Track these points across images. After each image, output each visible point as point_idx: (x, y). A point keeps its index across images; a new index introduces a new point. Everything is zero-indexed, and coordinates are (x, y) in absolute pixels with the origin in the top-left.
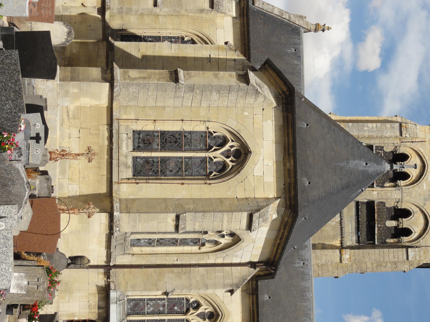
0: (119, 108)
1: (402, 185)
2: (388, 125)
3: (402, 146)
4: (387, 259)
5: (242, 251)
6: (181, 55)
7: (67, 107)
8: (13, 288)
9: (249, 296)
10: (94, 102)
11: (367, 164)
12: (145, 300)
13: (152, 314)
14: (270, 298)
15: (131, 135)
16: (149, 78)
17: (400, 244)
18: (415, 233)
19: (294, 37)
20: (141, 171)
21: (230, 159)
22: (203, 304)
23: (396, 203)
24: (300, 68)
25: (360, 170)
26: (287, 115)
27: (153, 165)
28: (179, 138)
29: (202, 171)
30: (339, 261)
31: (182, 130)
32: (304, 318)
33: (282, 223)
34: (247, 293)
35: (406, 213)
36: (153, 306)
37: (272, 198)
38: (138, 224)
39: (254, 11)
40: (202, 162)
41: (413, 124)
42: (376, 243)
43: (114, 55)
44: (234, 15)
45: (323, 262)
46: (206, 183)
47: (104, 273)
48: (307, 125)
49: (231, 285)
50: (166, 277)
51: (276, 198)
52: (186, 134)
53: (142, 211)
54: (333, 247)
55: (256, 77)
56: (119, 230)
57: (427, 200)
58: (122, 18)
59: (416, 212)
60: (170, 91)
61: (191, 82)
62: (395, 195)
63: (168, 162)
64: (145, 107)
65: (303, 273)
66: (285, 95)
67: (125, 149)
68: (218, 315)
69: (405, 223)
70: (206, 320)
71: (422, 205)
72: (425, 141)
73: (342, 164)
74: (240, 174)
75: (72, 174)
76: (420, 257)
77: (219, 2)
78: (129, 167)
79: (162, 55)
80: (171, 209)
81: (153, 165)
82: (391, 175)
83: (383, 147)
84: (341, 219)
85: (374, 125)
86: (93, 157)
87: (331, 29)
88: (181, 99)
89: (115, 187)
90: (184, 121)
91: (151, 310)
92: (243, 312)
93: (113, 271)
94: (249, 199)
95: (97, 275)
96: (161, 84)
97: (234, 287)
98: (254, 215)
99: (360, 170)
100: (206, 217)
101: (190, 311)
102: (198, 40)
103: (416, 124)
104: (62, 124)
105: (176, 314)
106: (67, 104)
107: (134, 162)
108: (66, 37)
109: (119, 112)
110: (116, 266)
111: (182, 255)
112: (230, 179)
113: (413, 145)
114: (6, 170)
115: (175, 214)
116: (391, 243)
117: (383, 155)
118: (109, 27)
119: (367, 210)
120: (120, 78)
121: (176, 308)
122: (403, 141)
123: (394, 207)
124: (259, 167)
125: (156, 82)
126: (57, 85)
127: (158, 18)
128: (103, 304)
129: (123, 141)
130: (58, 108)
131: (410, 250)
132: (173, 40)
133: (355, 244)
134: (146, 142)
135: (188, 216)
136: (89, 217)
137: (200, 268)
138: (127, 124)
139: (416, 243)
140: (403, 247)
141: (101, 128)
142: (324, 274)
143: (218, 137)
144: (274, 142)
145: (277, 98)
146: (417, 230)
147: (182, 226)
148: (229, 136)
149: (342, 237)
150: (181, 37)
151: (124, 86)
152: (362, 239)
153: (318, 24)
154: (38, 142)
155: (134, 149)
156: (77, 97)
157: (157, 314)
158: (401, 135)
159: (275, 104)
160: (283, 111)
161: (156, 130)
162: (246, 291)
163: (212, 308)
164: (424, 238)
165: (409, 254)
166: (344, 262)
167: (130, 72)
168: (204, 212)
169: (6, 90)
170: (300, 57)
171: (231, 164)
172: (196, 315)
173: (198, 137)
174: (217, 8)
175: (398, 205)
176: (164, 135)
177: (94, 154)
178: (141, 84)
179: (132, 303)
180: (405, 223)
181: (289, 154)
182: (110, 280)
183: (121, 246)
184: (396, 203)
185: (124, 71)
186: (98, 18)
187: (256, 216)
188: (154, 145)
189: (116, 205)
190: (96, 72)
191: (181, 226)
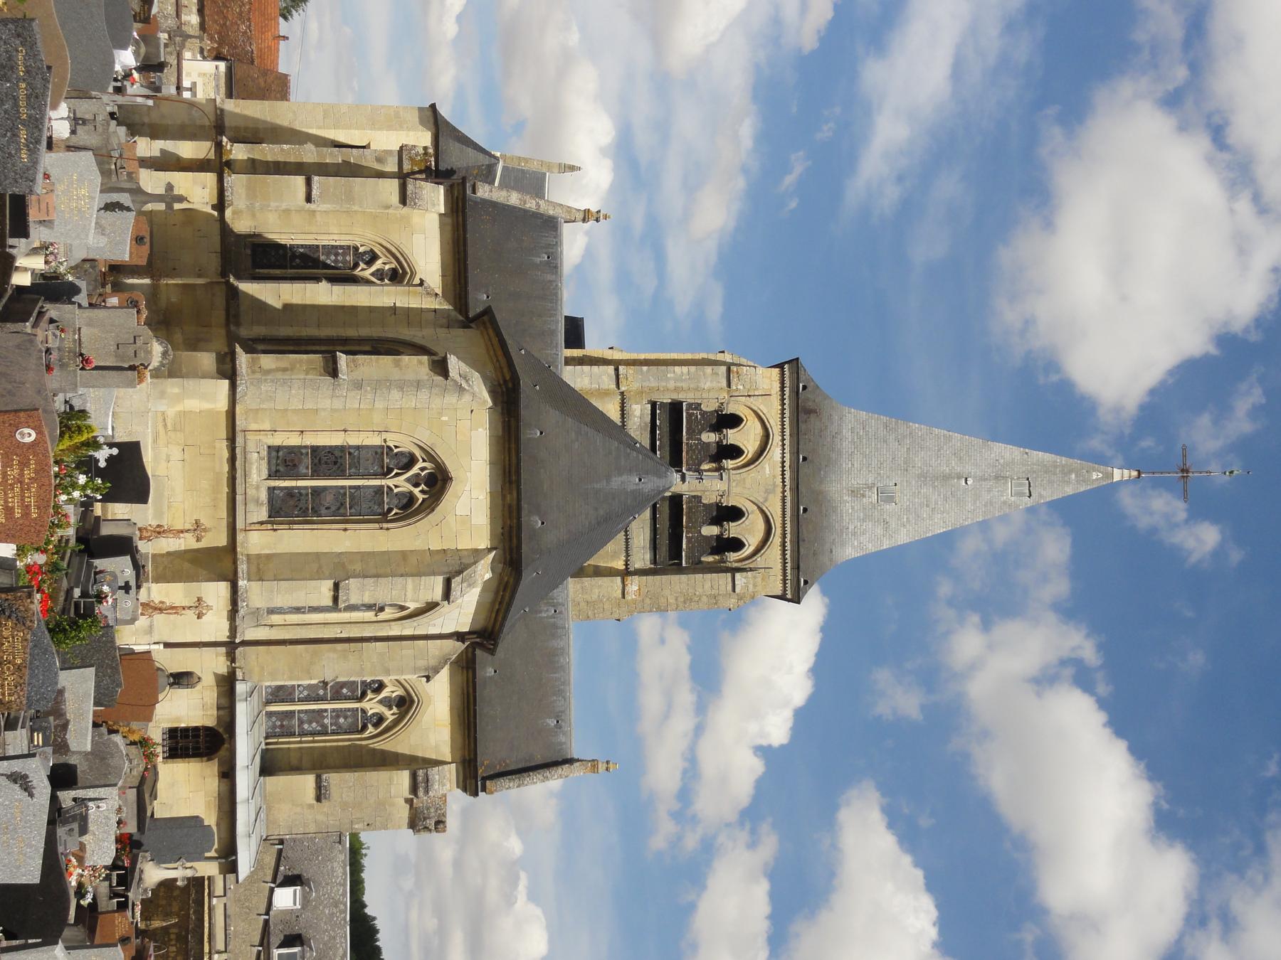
0: (246, 413)
1: (730, 467)
2: (708, 369)
3: (732, 402)
4: (699, 591)
5: (442, 619)
6: (347, 303)
7: (163, 413)
9: (463, 671)
10: (206, 406)
11: (640, 480)
13: (306, 701)
14: (495, 672)
15: (264, 453)
16: (292, 369)
17: (724, 565)
18: (749, 545)
19: (547, 235)
20: (281, 509)
21: (420, 488)
22: (387, 684)
23: (719, 498)
24: (557, 285)
25: (629, 490)
26: (509, 421)
27: (299, 500)
28: (341, 457)
29: (376, 507)
30: (621, 596)
31: (345, 444)
32: (555, 698)
33: (500, 583)
34: (459, 666)
35: (735, 514)
37: (484, 549)
38: (276, 595)
39: (476, 203)
41: (750, 366)
42: (684, 564)
43: (238, 305)
44: (442, 210)
45: (595, 597)
46: (381, 529)
47: (227, 653)
48: (541, 433)
49: (426, 669)
50: (323, 657)
51: (490, 550)
52: (352, 451)
53: (281, 577)
54: (611, 573)
55: (460, 362)
56: (246, 605)
57: (769, 493)
58: (254, 216)
59: (753, 512)
61: (357, 375)
62: (717, 485)
63: (324, 494)
64: (286, 410)
65: (555, 626)
66: (507, 388)
68: (412, 702)
69: (733, 529)
70: (392, 709)
73: (597, 486)
74: (435, 512)
75: (174, 518)
76: (755, 586)
77: (416, 193)
78: (262, 504)
79: (316, 303)
80: (327, 573)
81: (299, 500)
82: (713, 450)
83: (701, 404)
85: (685, 369)
86: (203, 534)
88: (343, 399)
90: (349, 432)
91: (305, 694)
93: (239, 651)
94: (449, 552)
95: (214, 657)
98: (453, 580)
99: (629, 490)
100: (380, 583)
101: (367, 695)
102: (382, 253)
103: (756, 365)
104: (155, 441)
105: (345, 700)
106: (162, 408)
107: (269, 494)
108: (160, 359)
109: (245, 419)
110: (245, 643)
111: (349, 625)
112: (419, 520)
113: (750, 401)
114: (104, 744)
115: (333, 581)
116: (708, 563)
117: (699, 417)
118: (232, 231)
119: (669, 509)
120: (247, 371)
121: (345, 691)
123: (717, 504)
124: (464, 499)
125: (302, 376)
127: (314, 215)
128: (224, 702)
129: (251, 464)
130: (150, 414)
131: (738, 576)
132: (340, 251)
133: (649, 565)
135: (353, 582)
136: (198, 618)
137: (378, 644)
138: (258, 438)
139: (749, 563)
140: (727, 570)
141: (218, 444)
142: (597, 616)
143: (402, 453)
144: (488, 462)
145: (493, 393)
146: (752, 542)
147: (344, 598)
148: (418, 453)
149: (628, 555)
150: (353, 247)
151: (252, 383)
152: (660, 558)
154: (127, 592)
155: (270, 476)
157: (314, 701)
158: (729, 385)
159: (490, 403)
160: (503, 414)
161: (303, 444)
163: (403, 690)
164: (762, 555)
165: (736, 583)
166: (628, 597)
167: (261, 360)
168: (377, 576)
169: (103, 667)
170: (556, 267)
171: (421, 497)
172: (377, 702)
173: (370, 454)
174: (413, 204)
177: (205, 530)
178: (278, 380)
180: (733, 529)
181: (510, 482)
182: (235, 664)
183: (251, 616)
184: (719, 498)
185: (252, 358)
186: (213, 215)
187: (456, 582)
188: (301, 468)
189: (242, 567)
190: (207, 360)
191: (342, 597)
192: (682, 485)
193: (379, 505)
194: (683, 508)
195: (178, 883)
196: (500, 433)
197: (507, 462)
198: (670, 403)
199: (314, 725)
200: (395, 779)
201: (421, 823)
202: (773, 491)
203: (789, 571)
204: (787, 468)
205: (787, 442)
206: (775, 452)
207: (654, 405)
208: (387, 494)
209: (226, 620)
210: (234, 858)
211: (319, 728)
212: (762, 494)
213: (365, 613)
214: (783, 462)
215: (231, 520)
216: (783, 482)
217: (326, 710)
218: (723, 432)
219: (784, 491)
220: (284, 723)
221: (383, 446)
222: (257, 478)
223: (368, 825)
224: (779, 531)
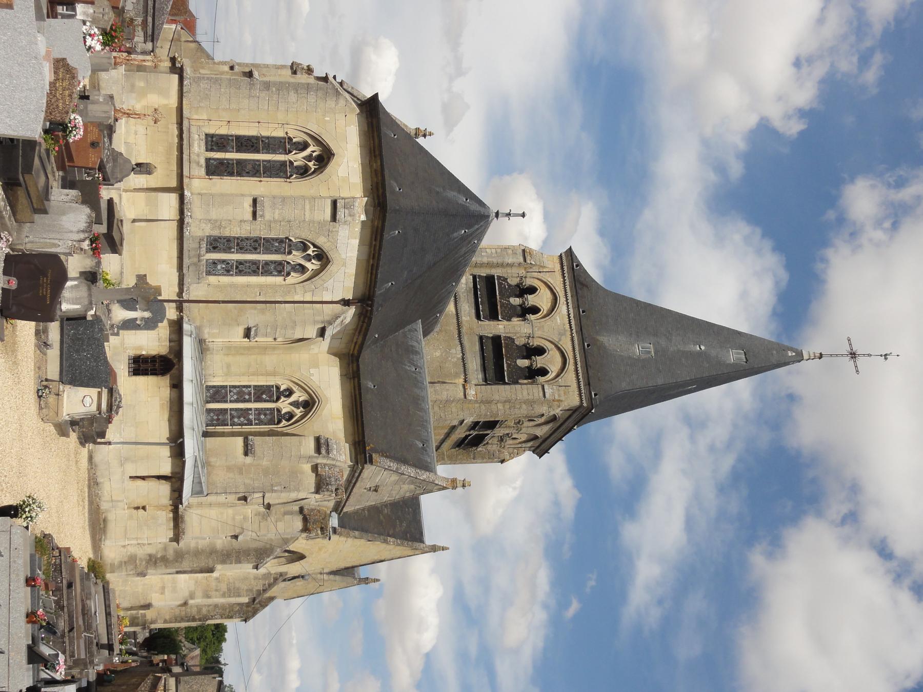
8: (80, 15)
10: (163, 101)
12: (227, 388)
15: (203, 137)
18: (552, 372)
23: (526, 340)
28: (256, 143)
31: (259, 135)
34: (347, 378)
35: (540, 351)
36: (238, 393)
40: (281, 165)
59: (552, 349)
60: (244, 89)
67: (197, 148)
72: (554, 272)
74: (323, 173)
84: (463, 354)
86: (159, 63)
87: (433, 134)
89: (186, 180)
92: (343, 398)
96: (234, 79)
97: (326, 324)
100: (286, 203)
117: (507, 287)
121: (264, 396)
122: (529, 271)
123: (525, 345)
126: (122, 74)
128: (174, 337)
134: (219, 145)
136: (155, 123)
141: (170, 126)
142: (447, 416)
143: (299, 143)
146: (554, 369)
148: (309, 141)
149: (466, 375)
153: (419, 128)
156: (143, 94)
158: (525, 260)
160: (367, 118)
162: (346, 375)
163: (307, 395)
165: (546, 391)
175: (529, 342)
176: (240, 139)
181: (375, 156)
184: (526, 340)
188: (229, 148)
191: (259, 213)
192: (500, 328)
193: (284, 173)
194: (502, 343)
195: (137, 322)
197: (372, 145)
198: (486, 277)
199: (242, 419)
200: (304, 442)
201: (325, 487)
202: (564, 334)
203: (582, 387)
204: (572, 318)
205: (570, 301)
206: (562, 308)
207: (474, 277)
208: (289, 166)
209: (176, 270)
210: (181, 440)
211: (246, 422)
212: (557, 336)
214: (569, 315)
215: (179, 171)
216: (571, 327)
217: (251, 409)
218: (524, 297)
219: (572, 334)
220: (220, 417)
221: (286, 138)
222: (198, 150)
224: (572, 361)
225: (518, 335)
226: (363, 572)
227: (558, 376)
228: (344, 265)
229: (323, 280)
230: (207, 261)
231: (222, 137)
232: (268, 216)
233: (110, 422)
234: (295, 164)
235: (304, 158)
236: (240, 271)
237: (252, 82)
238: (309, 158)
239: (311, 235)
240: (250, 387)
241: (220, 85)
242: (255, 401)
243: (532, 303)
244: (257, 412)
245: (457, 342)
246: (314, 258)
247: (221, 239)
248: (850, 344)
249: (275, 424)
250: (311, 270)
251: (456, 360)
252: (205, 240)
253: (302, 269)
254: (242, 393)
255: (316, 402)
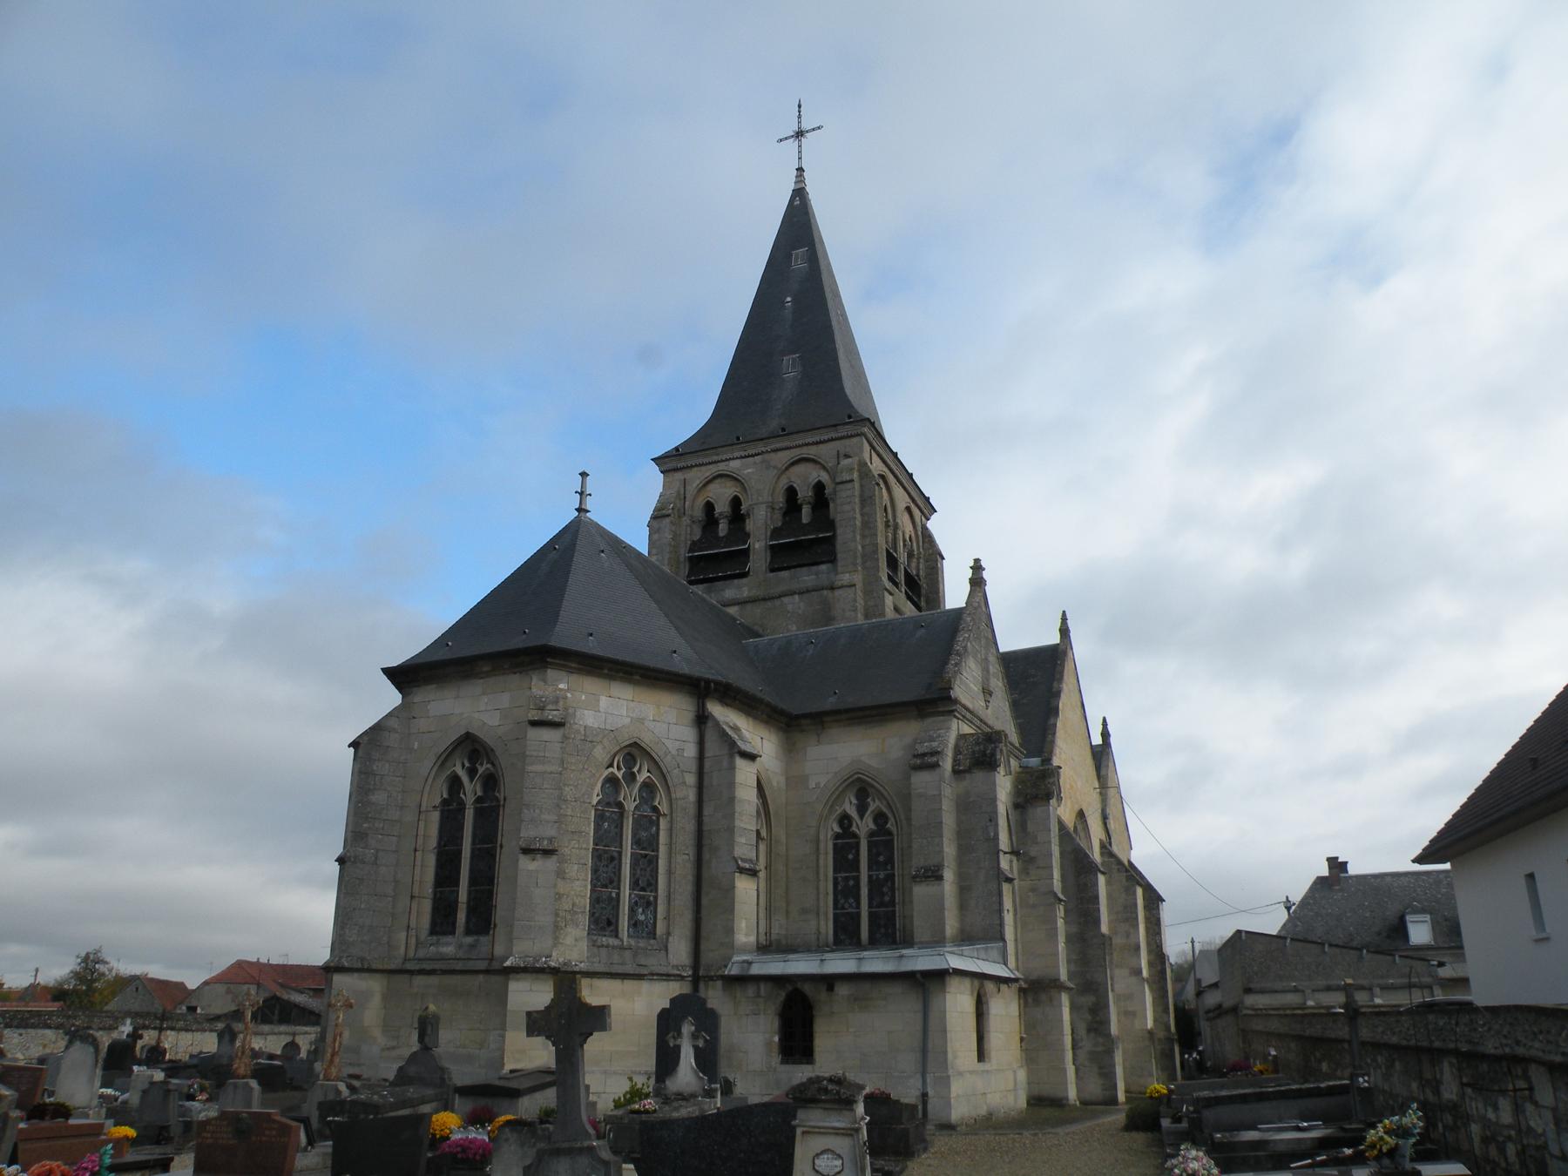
10: (376, 1001)
23: (776, 512)
31: (436, 851)
52: (443, 843)
71: (776, 471)
74: (494, 748)
146: (815, 475)
158: (668, 515)
160: (419, 686)
162: (818, 735)
179: (842, 937)
184: (776, 512)
192: (758, 545)
196: (434, 686)
199: (885, 889)
210: (918, 976)
211: (889, 884)
213: (661, 827)
214: (742, 457)
217: (870, 877)
223: (991, 820)
225: (769, 522)
226: (1097, 740)
227: (824, 468)
228: (641, 720)
229: (666, 755)
230: (632, 937)
231: (436, 909)
232: (550, 831)
233: (888, 1096)
234: (479, 793)
235: (472, 780)
236: (649, 884)
237: (352, 859)
238: (472, 772)
239: (590, 769)
240: (835, 879)
241: (354, 909)
242: (858, 869)
243: (727, 507)
244: (875, 868)
245: (777, 602)
246: (630, 769)
247: (594, 913)
248: (786, 138)
249: (892, 840)
250: (649, 774)
251: (802, 604)
252: (595, 938)
253: (648, 787)
254: (845, 891)
255: (859, 779)
